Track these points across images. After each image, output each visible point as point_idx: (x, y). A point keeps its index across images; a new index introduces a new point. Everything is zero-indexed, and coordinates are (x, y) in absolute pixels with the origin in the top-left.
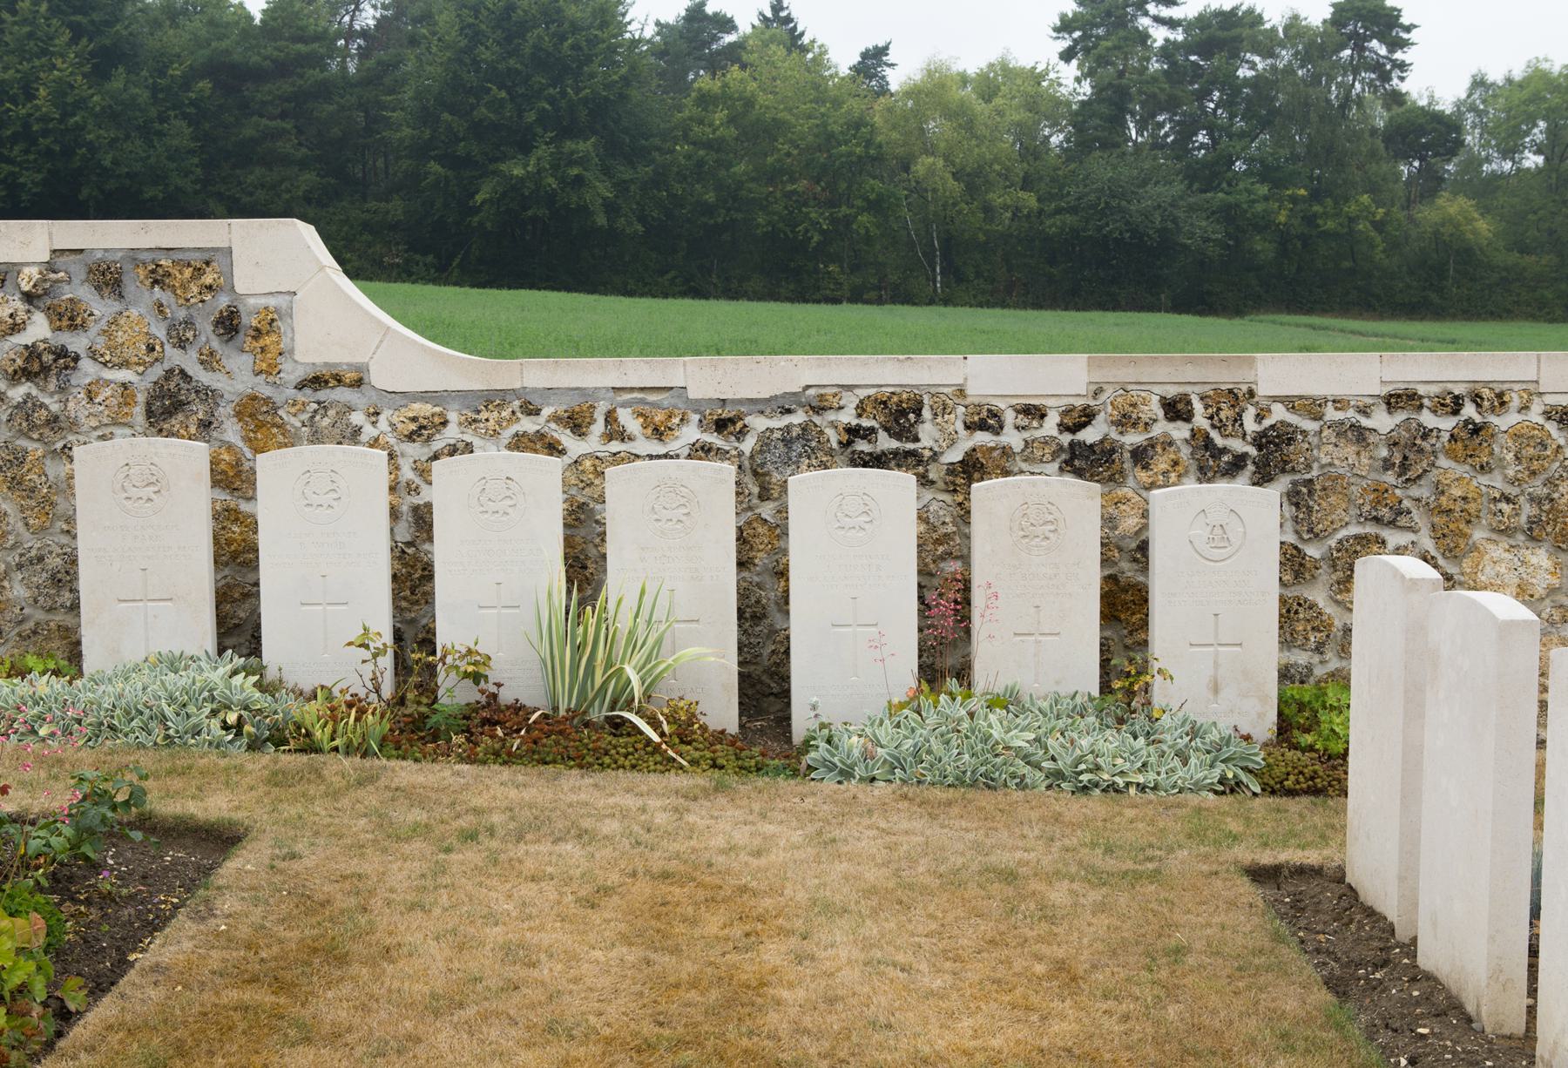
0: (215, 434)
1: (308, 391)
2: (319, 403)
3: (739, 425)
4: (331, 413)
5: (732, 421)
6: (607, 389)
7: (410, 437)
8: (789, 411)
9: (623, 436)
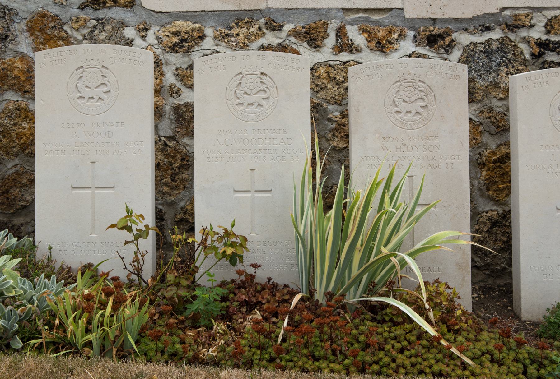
0: (10, 46)
1: (89, 10)
2: (98, 20)
3: (448, 40)
4: (108, 28)
5: (441, 36)
6: (338, 10)
7: (174, 48)
8: (488, 29)
9: (352, 48)
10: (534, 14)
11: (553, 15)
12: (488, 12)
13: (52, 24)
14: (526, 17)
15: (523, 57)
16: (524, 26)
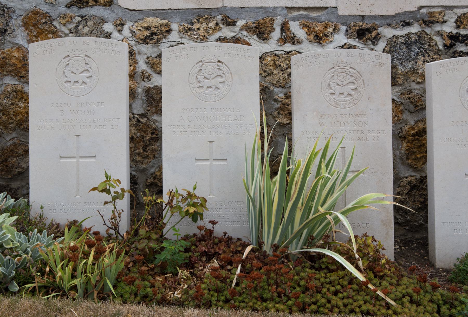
0: (8, 38)
2: (82, 17)
3: (374, 33)
4: (90, 23)
5: (369, 31)
6: (283, 8)
7: (145, 41)
8: (408, 24)
9: (294, 40)
10: (447, 12)
11: (462, 13)
12: (408, 10)
13: (44, 20)
14: (439, 14)
15: (437, 48)
16: (438, 22)
